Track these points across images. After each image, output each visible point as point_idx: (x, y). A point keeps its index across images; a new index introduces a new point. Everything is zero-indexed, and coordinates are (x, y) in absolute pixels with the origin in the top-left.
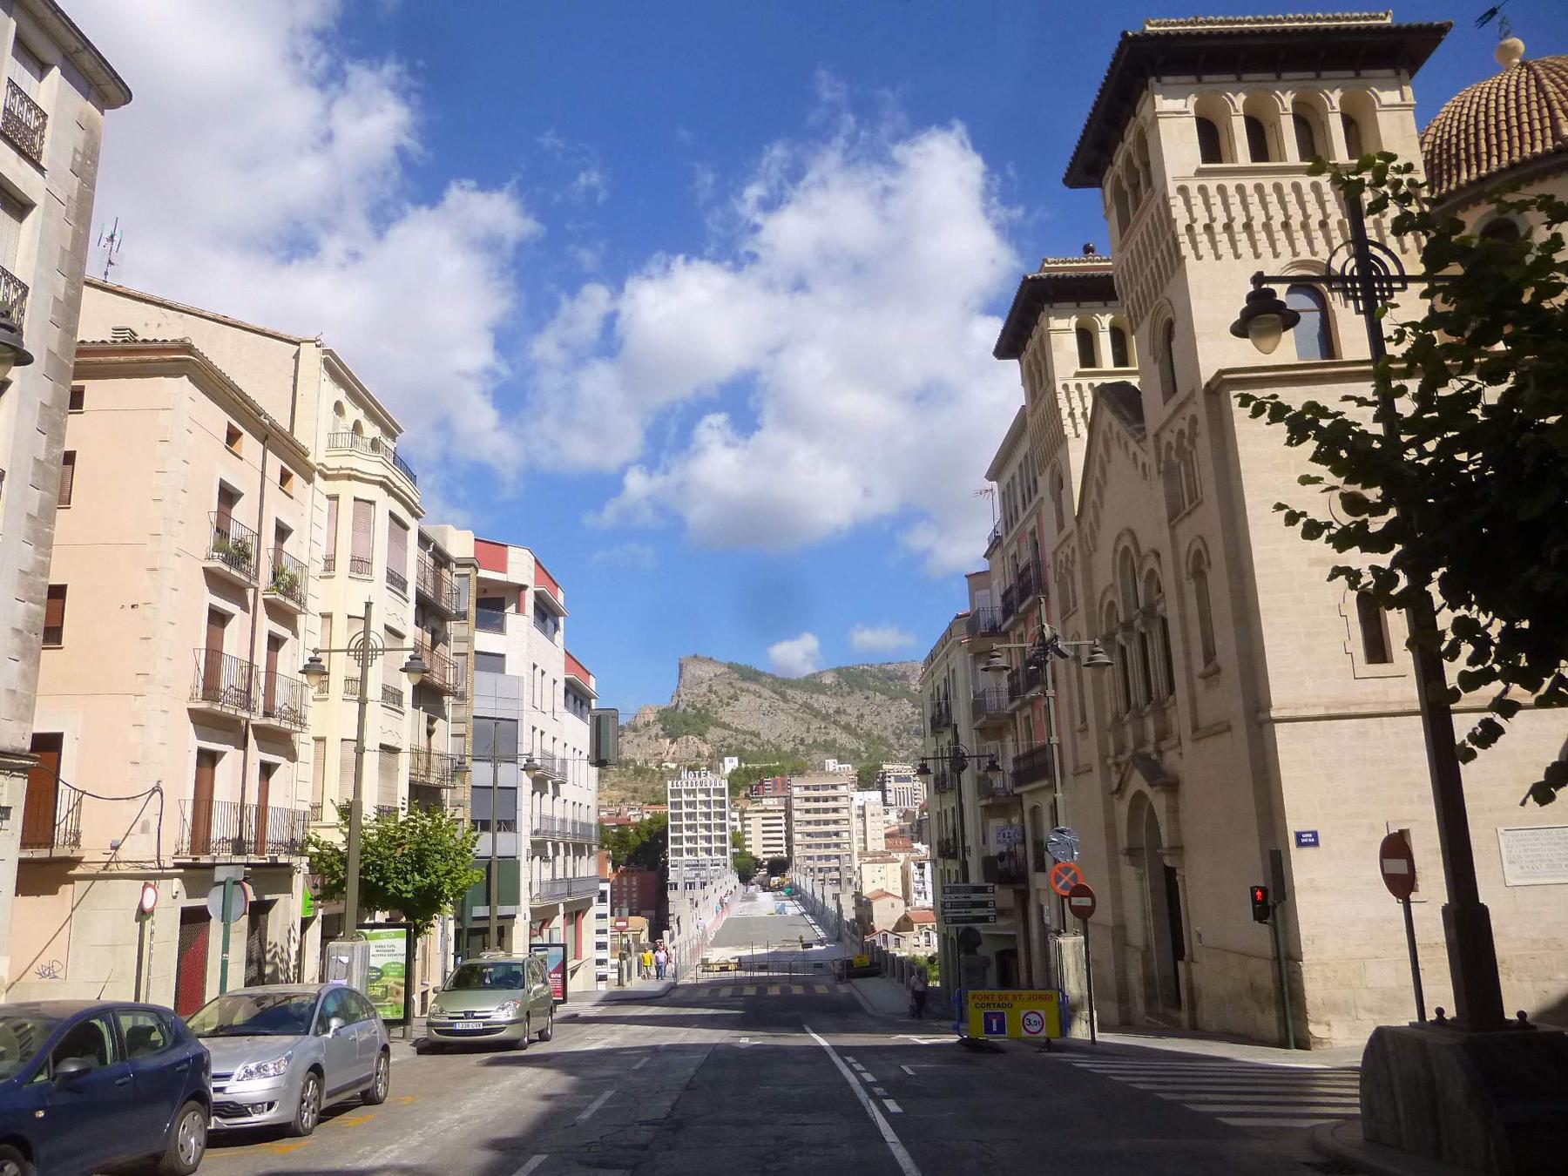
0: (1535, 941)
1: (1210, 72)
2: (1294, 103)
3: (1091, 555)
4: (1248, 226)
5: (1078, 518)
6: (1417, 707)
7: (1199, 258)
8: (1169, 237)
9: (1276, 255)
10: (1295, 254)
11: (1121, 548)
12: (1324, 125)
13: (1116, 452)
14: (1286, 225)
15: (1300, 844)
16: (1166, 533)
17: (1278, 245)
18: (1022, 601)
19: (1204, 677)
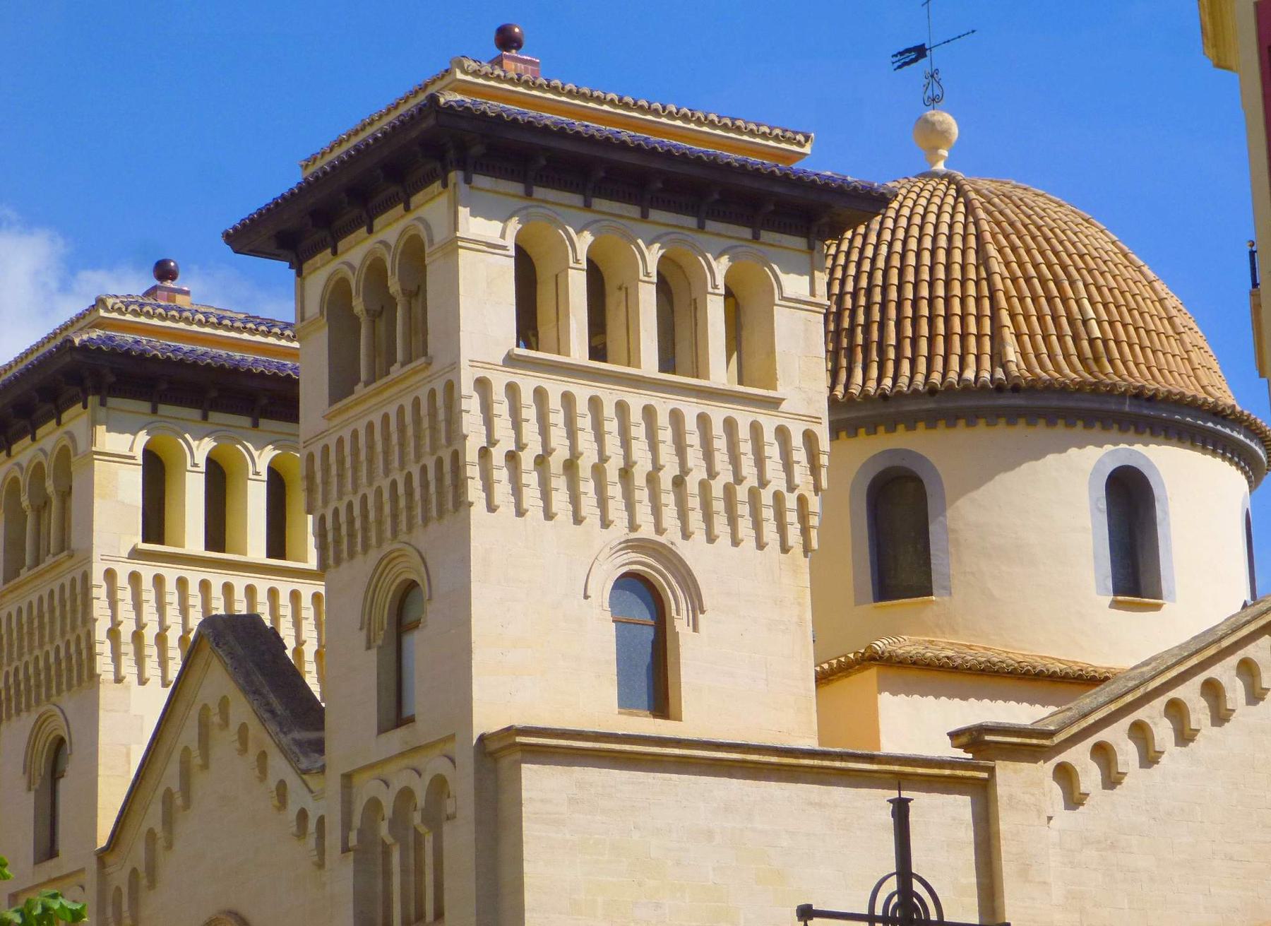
2: (663, 260)
4: (570, 466)
7: (491, 508)
10: (633, 527)
12: (696, 309)
13: (224, 744)
17: (612, 505)
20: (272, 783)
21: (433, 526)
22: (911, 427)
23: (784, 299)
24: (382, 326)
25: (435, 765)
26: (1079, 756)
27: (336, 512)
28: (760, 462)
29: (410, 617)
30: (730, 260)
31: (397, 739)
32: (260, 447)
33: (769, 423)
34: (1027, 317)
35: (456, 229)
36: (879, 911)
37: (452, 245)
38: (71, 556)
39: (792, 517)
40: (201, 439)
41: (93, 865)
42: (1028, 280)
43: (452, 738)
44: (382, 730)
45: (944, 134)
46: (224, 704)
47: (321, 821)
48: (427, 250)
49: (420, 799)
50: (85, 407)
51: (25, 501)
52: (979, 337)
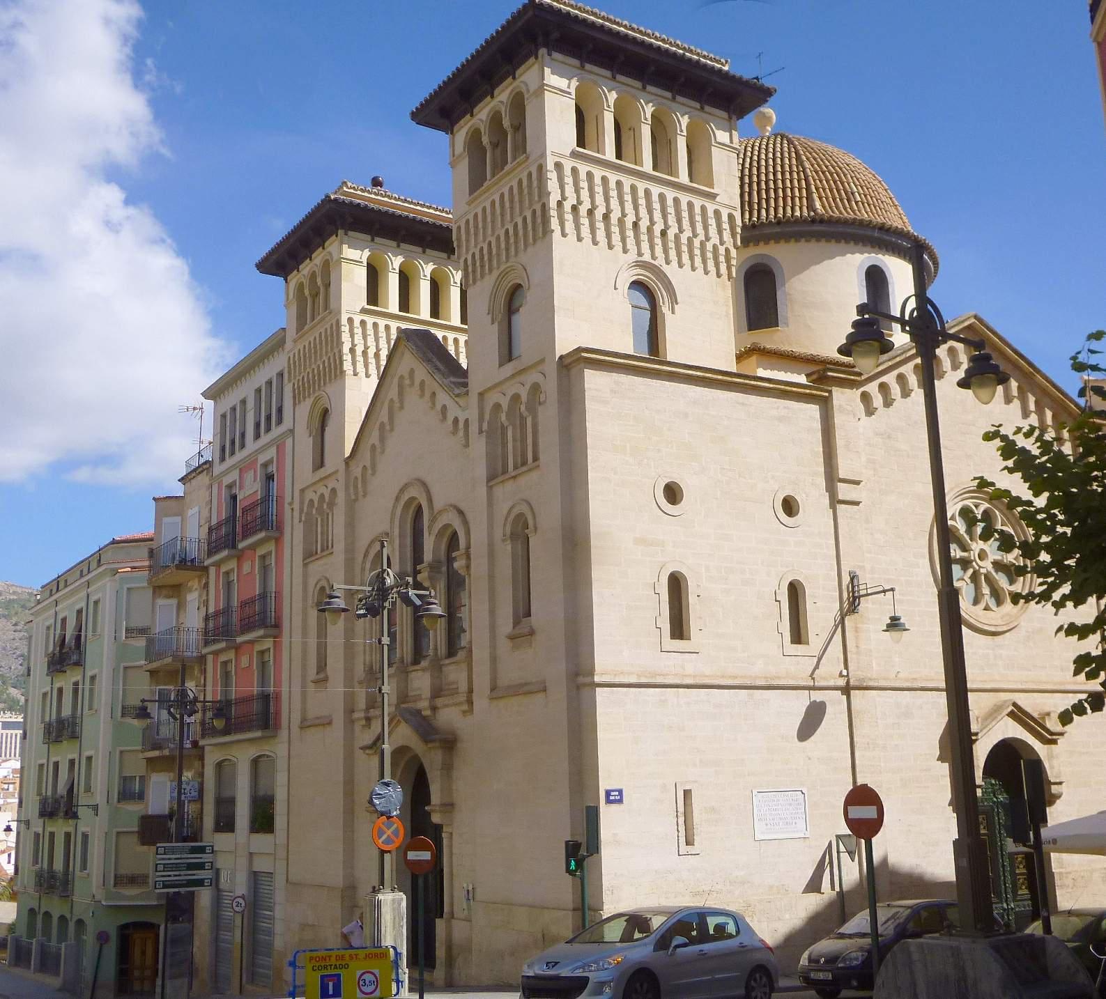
0: (771, 887)
1: (561, 51)
3: (356, 500)
5: (348, 461)
6: (943, 685)
7: (564, 235)
8: (538, 207)
9: (625, 251)
10: (640, 254)
11: (406, 497)
13: (412, 396)
14: (636, 225)
15: (608, 801)
16: (482, 491)
18: (245, 537)
19: (512, 638)
20: (439, 407)
21: (530, 249)
22: (767, 243)
23: (720, 143)
24: (498, 151)
25: (533, 377)
26: (872, 388)
27: (473, 255)
28: (706, 228)
29: (516, 304)
30: (689, 118)
31: (509, 369)
32: (427, 263)
33: (711, 208)
34: (824, 190)
35: (543, 79)
37: (541, 88)
38: (330, 313)
39: (722, 259)
40: (396, 256)
41: (342, 467)
42: (823, 173)
43: (542, 361)
44: (501, 365)
45: (770, 118)
46: (412, 372)
47: (467, 421)
48: (526, 96)
49: (524, 398)
50: (337, 236)
51: (307, 292)
52: (800, 198)
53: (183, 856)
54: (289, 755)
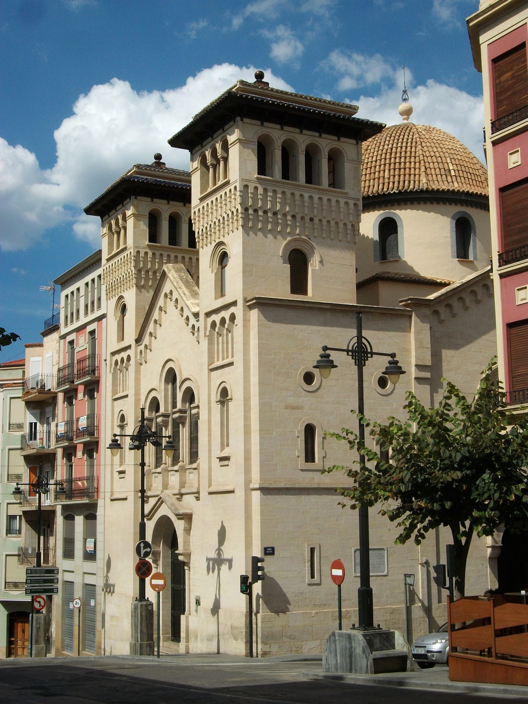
20: (185, 317)
23: (349, 160)
36: (350, 348)
44: (216, 298)
53: (41, 575)
54: (521, 109)
